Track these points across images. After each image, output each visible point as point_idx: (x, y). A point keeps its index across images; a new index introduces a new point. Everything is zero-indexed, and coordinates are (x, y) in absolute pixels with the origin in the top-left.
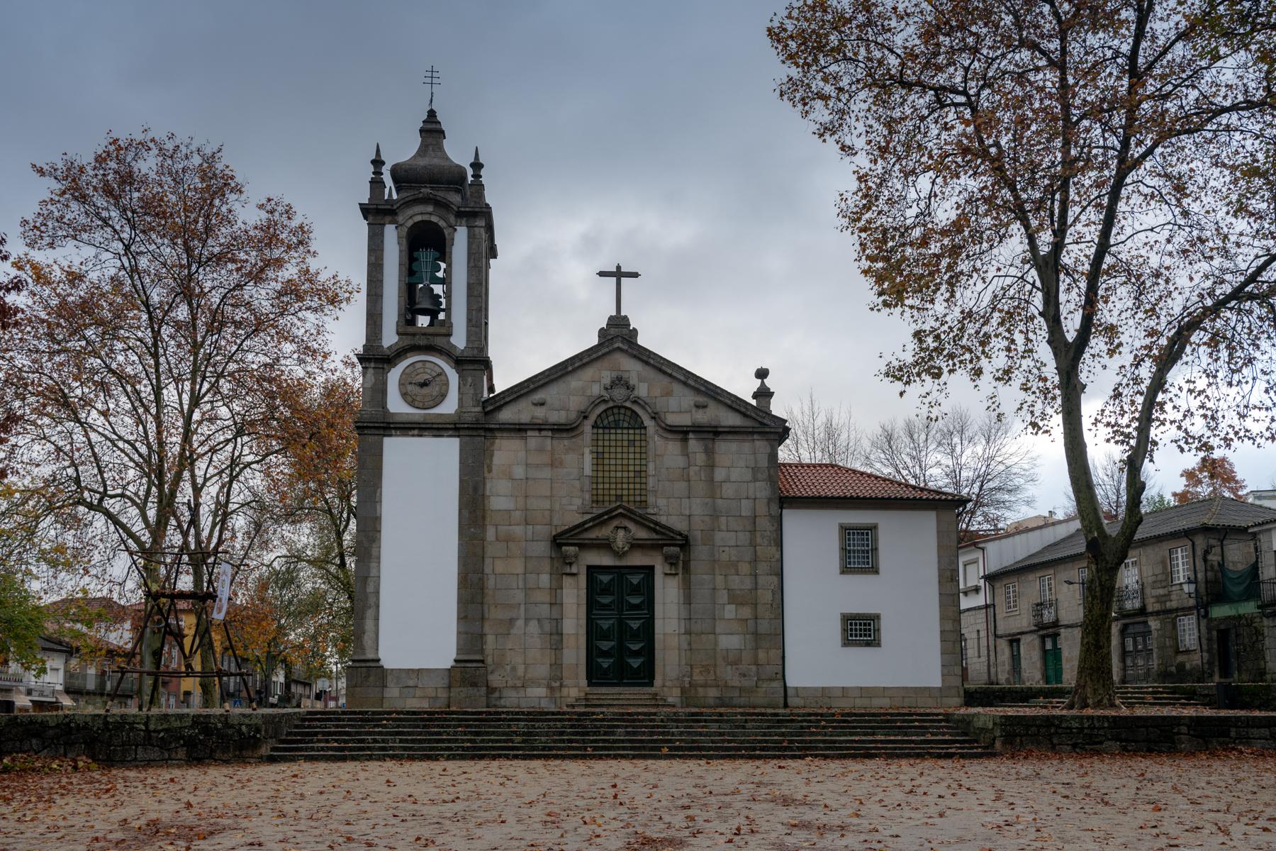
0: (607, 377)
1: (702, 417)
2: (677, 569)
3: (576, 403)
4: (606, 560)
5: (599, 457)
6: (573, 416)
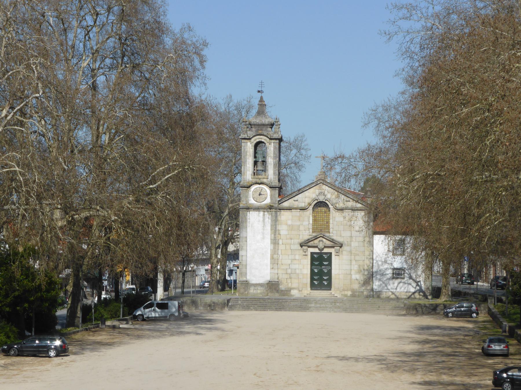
0: (317, 192)
2: (31, 333)
3: (308, 201)
4: (316, 250)
5: (315, 217)
6: (306, 204)
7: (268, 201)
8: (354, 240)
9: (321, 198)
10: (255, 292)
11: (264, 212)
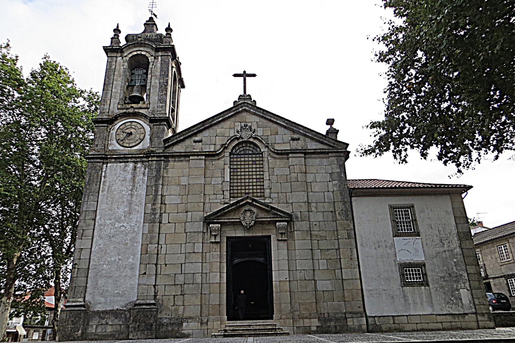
3: (220, 141)
4: (240, 233)
7: (146, 144)
8: (313, 209)
9: (246, 135)
10: (99, 330)
11: (136, 162)
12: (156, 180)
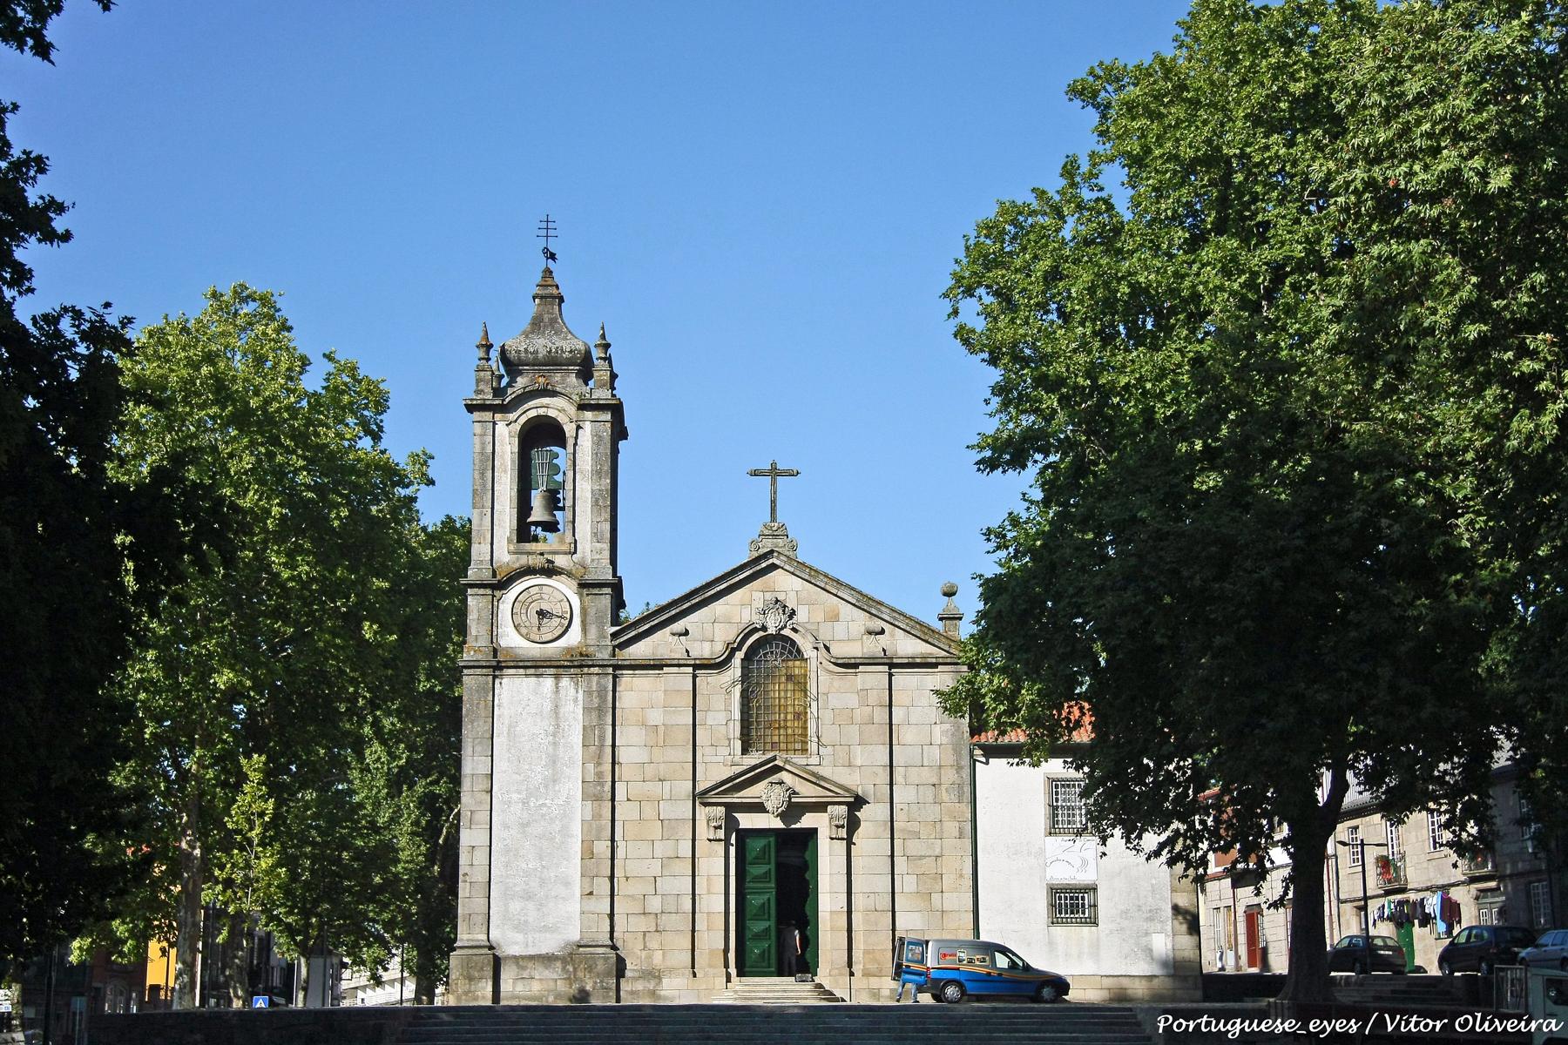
1: (873, 647)
3: (725, 634)
12: (606, 712)
